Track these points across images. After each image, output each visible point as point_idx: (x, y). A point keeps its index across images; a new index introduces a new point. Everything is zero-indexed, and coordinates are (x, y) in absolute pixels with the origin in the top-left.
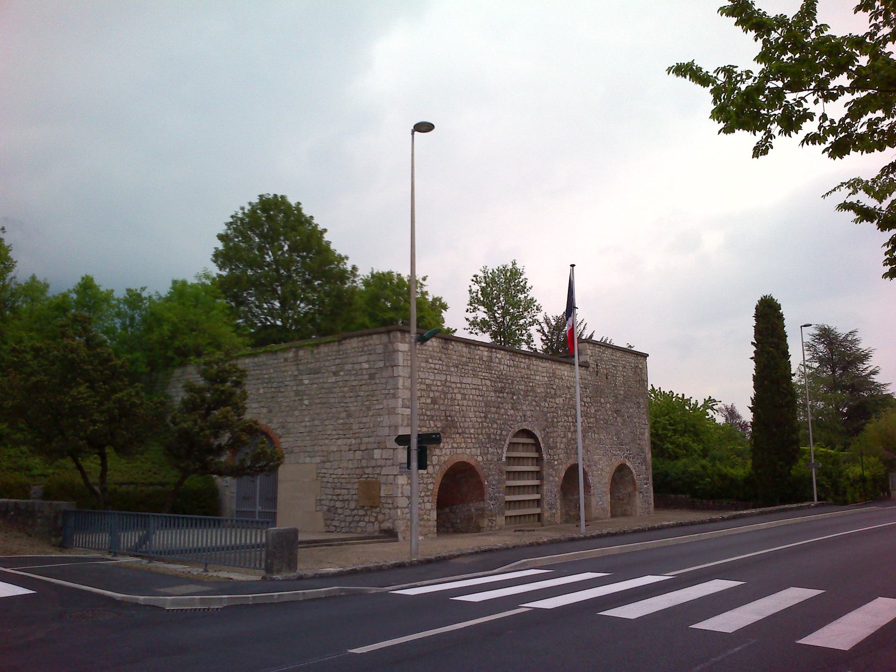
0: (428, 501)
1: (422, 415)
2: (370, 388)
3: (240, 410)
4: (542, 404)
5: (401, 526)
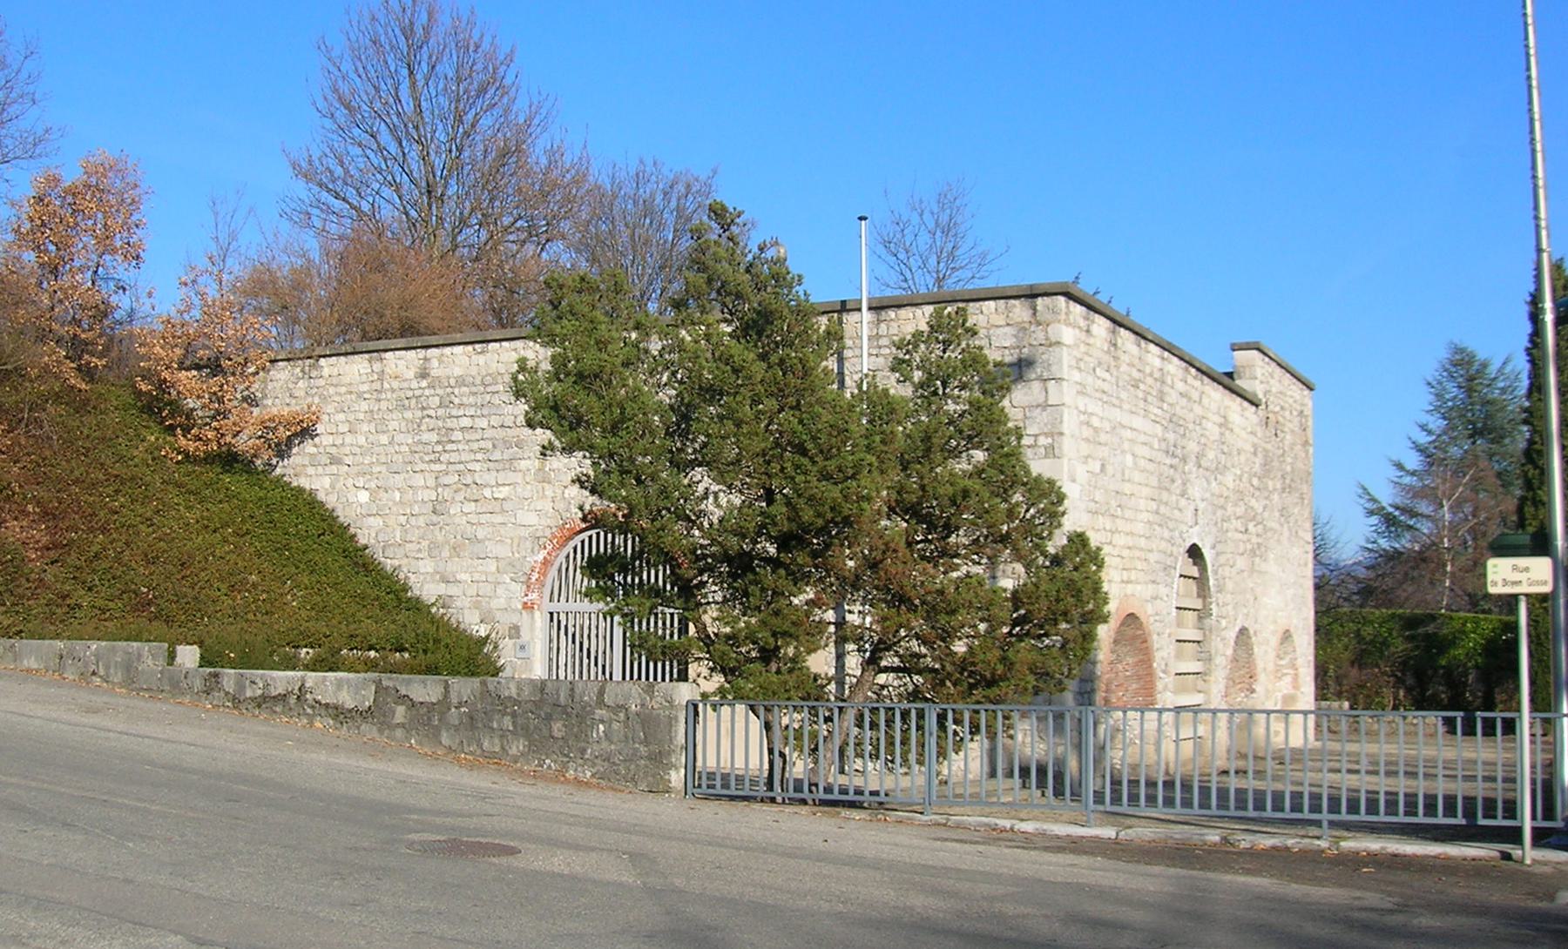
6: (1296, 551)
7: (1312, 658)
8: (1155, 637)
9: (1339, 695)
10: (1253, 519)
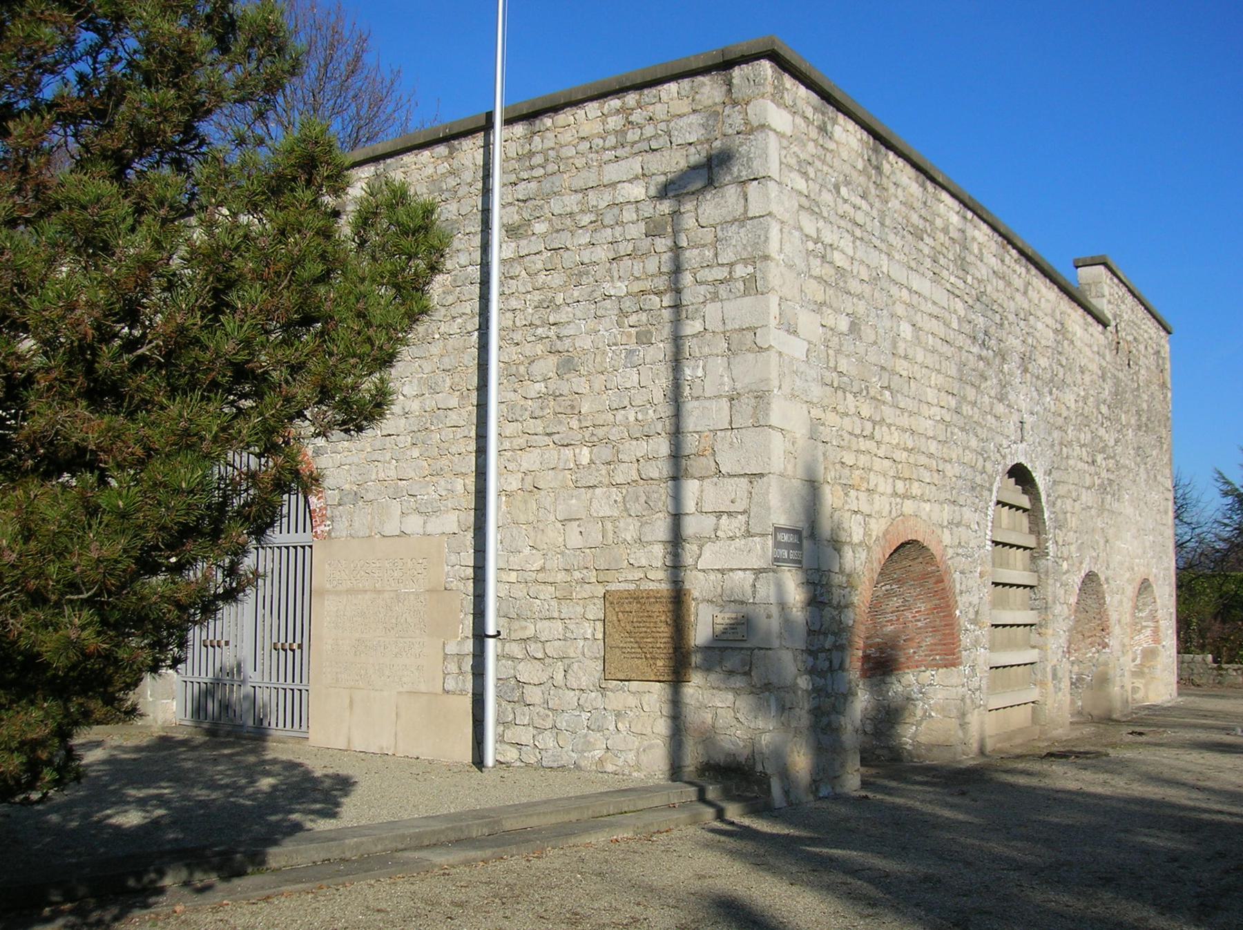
6: (1155, 496)
7: (1173, 610)
8: (957, 576)
9: (1202, 648)
10: (1103, 450)
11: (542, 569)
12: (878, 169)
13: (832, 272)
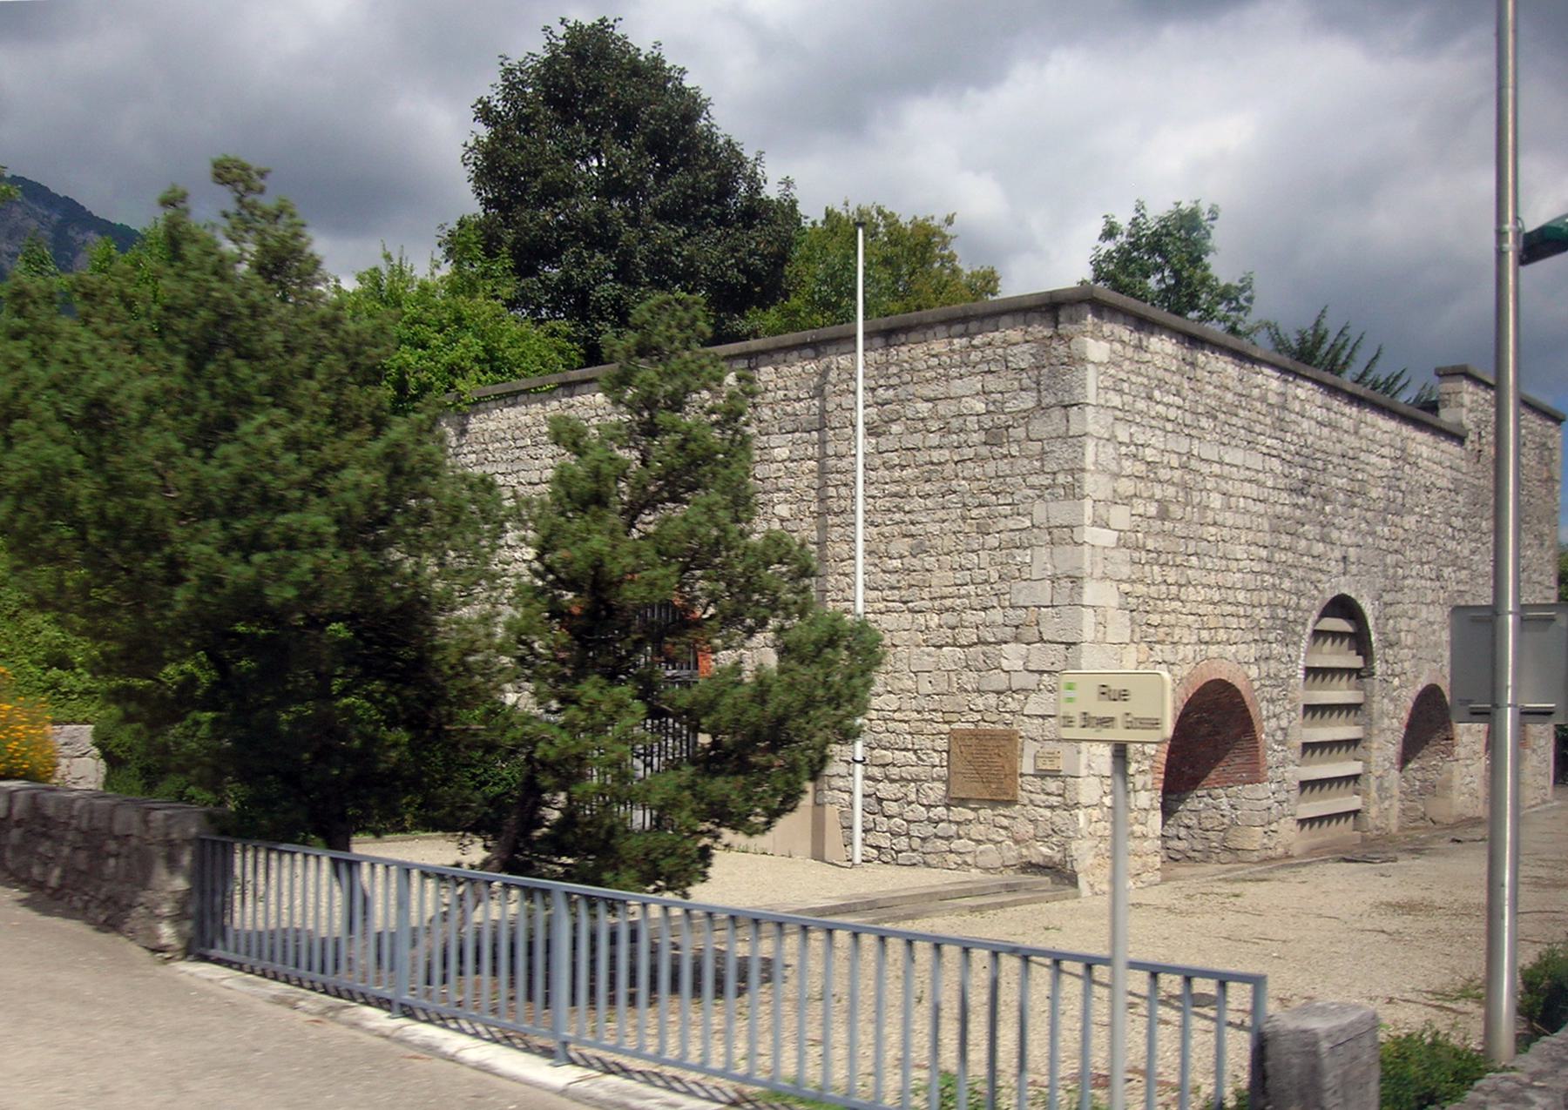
0: (1144, 788)
1: (1137, 548)
2: (990, 468)
3: (742, 504)
4: (1379, 529)
5: (1086, 857)
11: (899, 709)
12: (1193, 365)
13: (1143, 467)
